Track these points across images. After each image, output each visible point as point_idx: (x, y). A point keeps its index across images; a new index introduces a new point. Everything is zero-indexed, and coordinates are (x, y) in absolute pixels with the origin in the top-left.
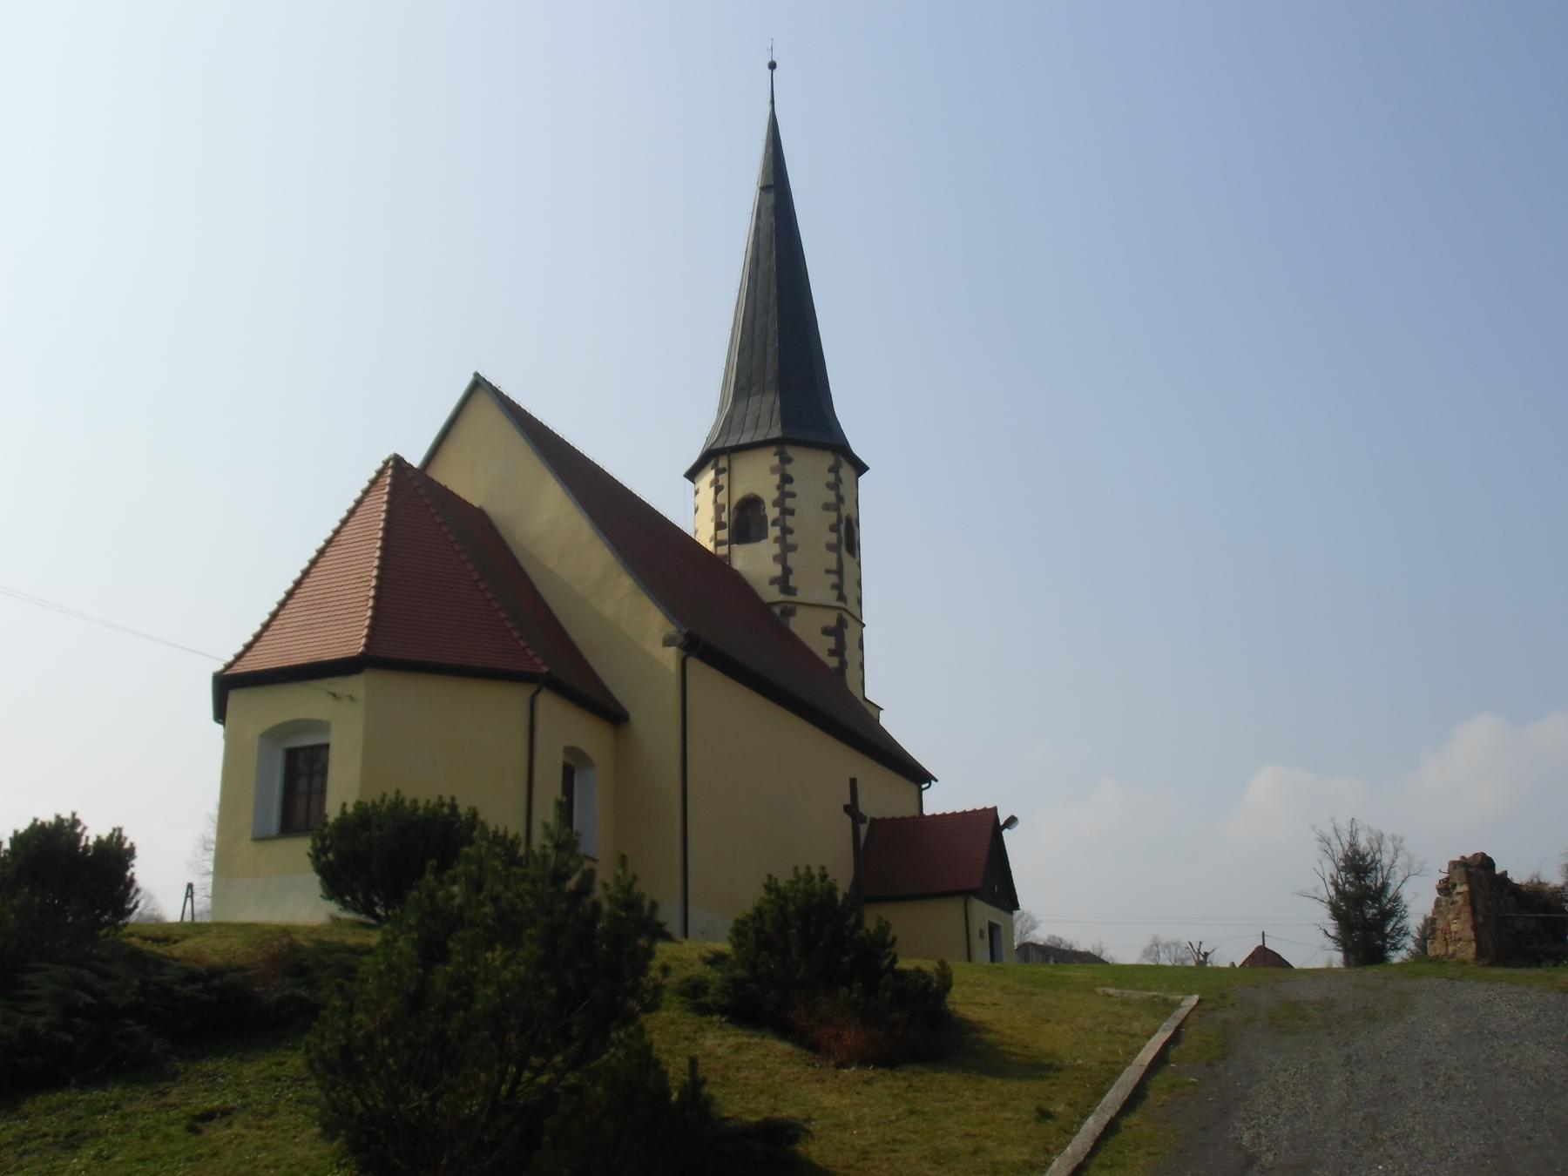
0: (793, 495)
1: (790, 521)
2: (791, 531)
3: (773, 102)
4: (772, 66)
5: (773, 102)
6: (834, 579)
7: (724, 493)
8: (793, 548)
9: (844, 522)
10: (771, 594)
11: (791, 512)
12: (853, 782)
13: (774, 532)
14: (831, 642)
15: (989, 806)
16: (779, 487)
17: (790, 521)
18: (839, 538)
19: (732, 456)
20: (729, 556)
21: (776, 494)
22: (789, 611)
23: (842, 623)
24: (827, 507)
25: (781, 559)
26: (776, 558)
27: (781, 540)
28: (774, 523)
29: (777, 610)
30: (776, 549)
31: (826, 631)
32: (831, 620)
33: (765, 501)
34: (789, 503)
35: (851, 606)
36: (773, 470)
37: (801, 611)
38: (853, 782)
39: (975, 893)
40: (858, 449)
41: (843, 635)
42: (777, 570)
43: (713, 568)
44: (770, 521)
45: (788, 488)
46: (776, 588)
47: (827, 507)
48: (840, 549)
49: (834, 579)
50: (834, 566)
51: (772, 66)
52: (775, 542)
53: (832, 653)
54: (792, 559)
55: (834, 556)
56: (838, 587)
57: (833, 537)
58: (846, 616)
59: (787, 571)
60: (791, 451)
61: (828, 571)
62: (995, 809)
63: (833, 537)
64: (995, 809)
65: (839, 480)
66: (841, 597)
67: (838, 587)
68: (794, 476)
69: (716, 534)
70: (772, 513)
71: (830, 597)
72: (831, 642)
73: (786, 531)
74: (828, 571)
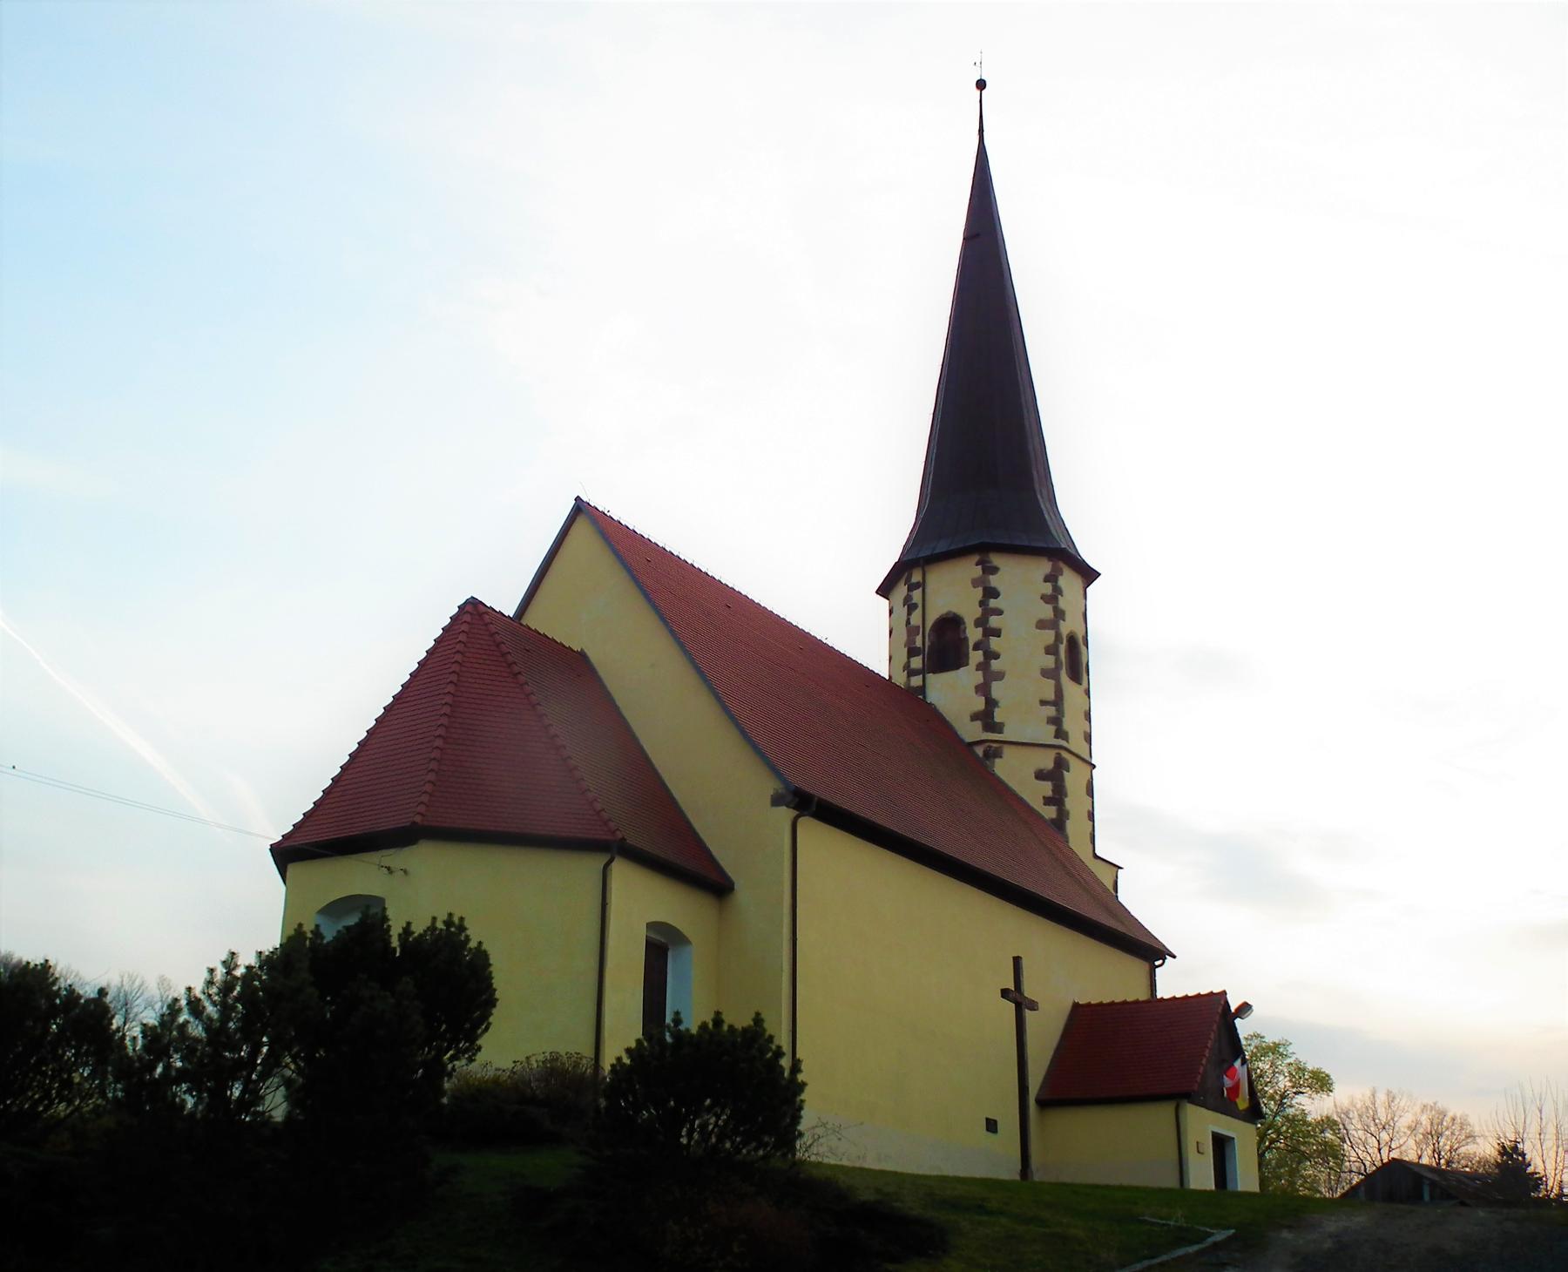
0: (999, 612)
1: (994, 643)
2: (997, 656)
4: (981, 85)
6: (1051, 711)
9: (1065, 641)
10: (971, 731)
11: (997, 633)
12: (1017, 961)
13: (976, 657)
14: (1047, 788)
16: (982, 603)
17: (994, 643)
18: (1058, 661)
19: (926, 568)
20: (922, 689)
21: (978, 612)
22: (993, 753)
24: (1041, 625)
25: (983, 689)
27: (983, 667)
28: (977, 647)
29: (979, 751)
30: (979, 677)
31: (1041, 775)
32: (1047, 761)
33: (966, 620)
34: (994, 621)
35: (1076, 743)
37: (1008, 751)
38: (1017, 961)
42: (979, 704)
45: (993, 603)
46: (978, 724)
47: (1041, 625)
49: (1051, 711)
50: (1051, 696)
51: (981, 85)
52: (977, 670)
53: (1048, 801)
54: (997, 689)
56: (1056, 721)
58: (1065, 755)
59: (991, 704)
60: (996, 560)
61: (1043, 703)
62: (1224, 993)
63: (1049, 661)
65: (1057, 591)
66: (1061, 733)
68: (1000, 588)
70: (973, 634)
71: (1047, 734)
72: (1047, 788)
73: (991, 655)
74: (1043, 703)
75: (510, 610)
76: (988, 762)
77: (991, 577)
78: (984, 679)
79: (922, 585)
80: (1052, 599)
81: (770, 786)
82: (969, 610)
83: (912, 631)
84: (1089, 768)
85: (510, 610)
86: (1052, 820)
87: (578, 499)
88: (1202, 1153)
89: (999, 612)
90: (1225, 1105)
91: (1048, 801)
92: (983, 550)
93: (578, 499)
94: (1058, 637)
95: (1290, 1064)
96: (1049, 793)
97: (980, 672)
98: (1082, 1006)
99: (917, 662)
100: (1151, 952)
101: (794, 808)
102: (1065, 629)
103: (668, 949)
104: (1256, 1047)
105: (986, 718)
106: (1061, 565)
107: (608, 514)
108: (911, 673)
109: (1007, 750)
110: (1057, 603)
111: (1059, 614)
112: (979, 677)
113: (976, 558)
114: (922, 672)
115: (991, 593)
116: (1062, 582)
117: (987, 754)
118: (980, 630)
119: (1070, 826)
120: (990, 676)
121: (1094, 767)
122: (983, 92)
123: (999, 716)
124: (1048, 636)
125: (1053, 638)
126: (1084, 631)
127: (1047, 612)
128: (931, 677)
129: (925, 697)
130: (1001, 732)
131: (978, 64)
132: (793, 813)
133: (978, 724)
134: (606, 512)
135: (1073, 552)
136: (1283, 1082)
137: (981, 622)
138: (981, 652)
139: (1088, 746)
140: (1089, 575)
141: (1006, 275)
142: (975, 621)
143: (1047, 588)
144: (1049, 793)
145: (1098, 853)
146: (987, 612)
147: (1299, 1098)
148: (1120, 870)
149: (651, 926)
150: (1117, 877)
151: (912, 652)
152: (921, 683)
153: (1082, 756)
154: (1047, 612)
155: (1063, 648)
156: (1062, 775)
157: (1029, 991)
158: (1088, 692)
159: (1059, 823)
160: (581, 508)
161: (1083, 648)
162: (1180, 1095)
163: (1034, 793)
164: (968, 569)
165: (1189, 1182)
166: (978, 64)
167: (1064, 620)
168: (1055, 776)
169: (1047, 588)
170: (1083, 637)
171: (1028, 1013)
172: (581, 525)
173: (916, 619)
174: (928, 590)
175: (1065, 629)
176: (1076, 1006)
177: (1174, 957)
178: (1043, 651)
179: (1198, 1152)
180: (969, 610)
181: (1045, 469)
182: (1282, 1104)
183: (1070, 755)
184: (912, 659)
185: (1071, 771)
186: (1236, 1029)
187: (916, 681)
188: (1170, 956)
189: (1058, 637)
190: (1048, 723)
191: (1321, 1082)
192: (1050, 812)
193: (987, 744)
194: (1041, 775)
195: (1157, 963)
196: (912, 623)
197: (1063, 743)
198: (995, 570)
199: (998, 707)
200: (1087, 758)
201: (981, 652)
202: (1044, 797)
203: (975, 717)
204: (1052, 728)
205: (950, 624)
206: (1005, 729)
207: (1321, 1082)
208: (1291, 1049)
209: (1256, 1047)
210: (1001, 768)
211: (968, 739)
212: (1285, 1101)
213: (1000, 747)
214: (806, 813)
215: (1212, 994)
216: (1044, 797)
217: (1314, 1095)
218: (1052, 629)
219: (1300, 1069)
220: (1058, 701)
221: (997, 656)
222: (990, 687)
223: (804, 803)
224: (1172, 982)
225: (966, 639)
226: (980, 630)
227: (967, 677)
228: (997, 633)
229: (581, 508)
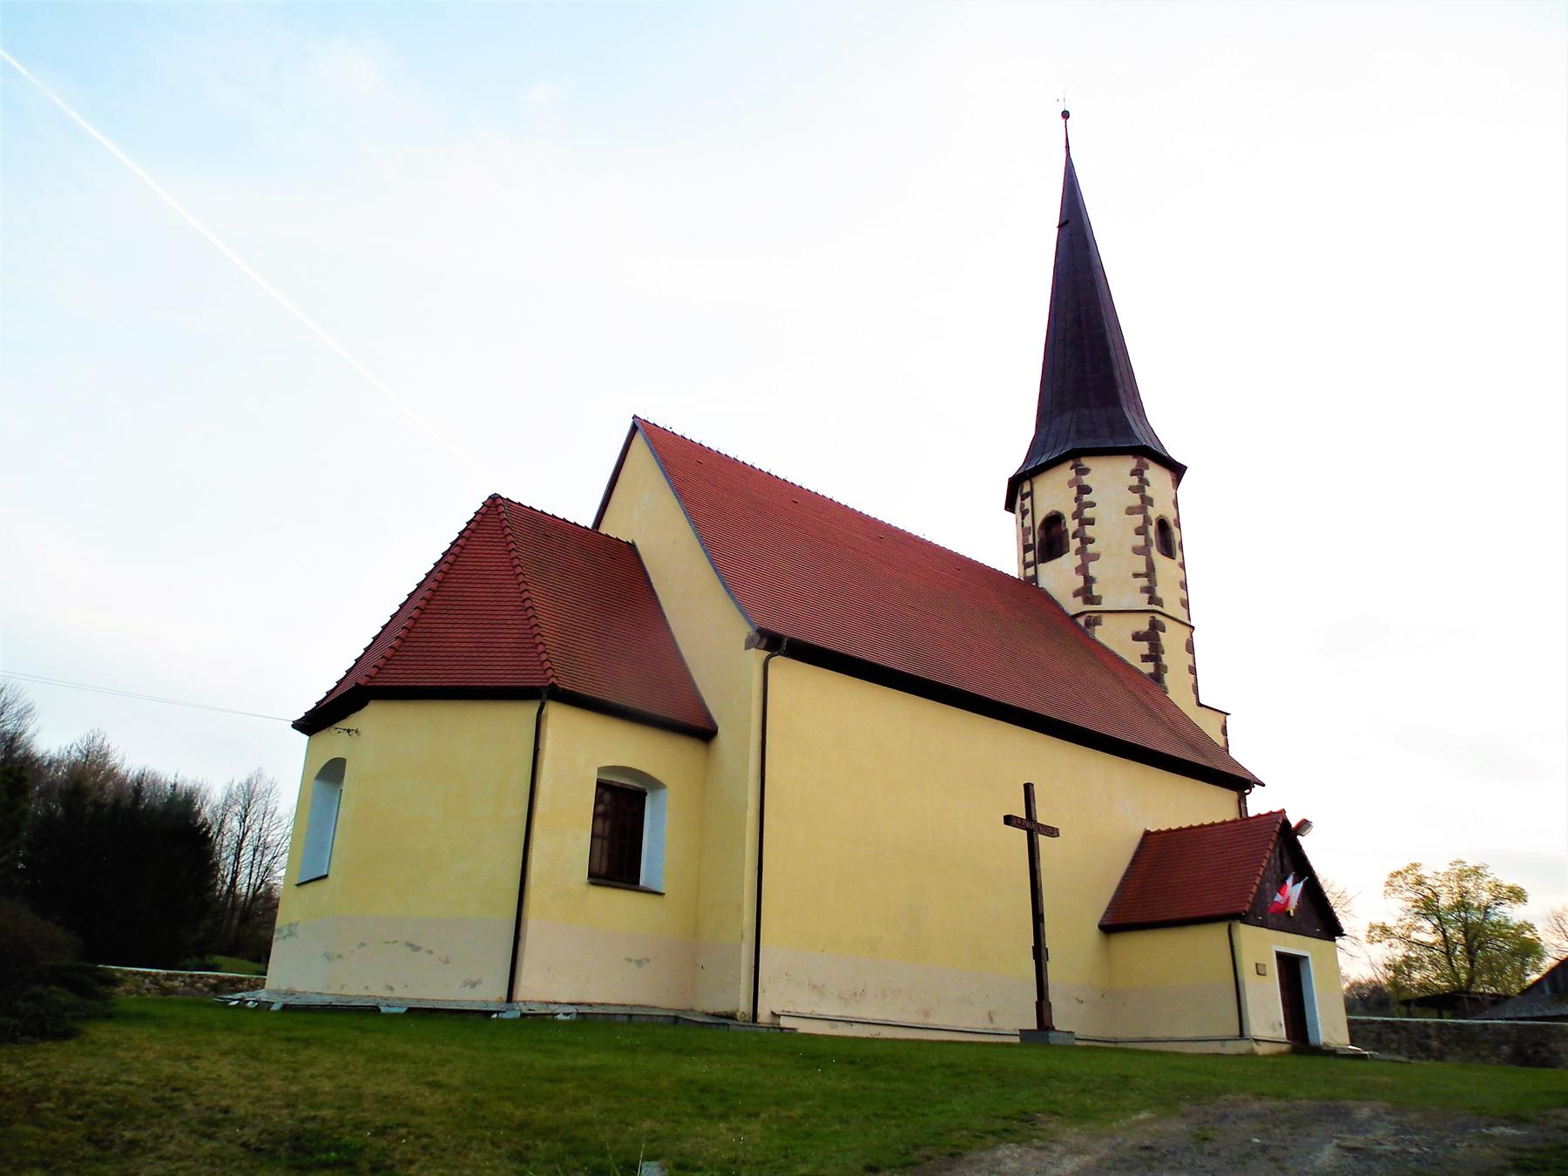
0: (1092, 505)
1: (1089, 531)
2: (1092, 541)
3: (1067, 147)
4: (1066, 115)
5: (1067, 147)
6: (1144, 582)
7: (1028, 517)
8: (1096, 557)
9: (1154, 523)
10: (1073, 606)
11: (1091, 522)
12: (1028, 788)
13: (1075, 544)
14: (1144, 647)
15: (1275, 810)
16: (1077, 500)
17: (1089, 531)
18: (1147, 540)
19: (1033, 480)
20: (1035, 578)
21: (1074, 507)
22: (1093, 622)
23: (1156, 627)
24: (1131, 511)
25: (1082, 570)
26: (1077, 570)
27: (1081, 551)
28: (1074, 536)
29: (1081, 621)
30: (1078, 560)
31: (1137, 637)
32: (1143, 624)
33: (1066, 516)
34: (1088, 513)
35: (1171, 606)
36: (1071, 484)
37: (1105, 618)
38: (1028, 788)
39: (1245, 919)
40: (1175, 452)
41: (1158, 639)
42: (1079, 582)
43: (1027, 590)
44: (1070, 534)
45: (1086, 498)
46: (1080, 599)
47: (1131, 511)
48: (1149, 551)
49: (1144, 582)
50: (1143, 569)
51: (1066, 115)
52: (1076, 554)
53: (1145, 658)
54: (1093, 569)
55: (1143, 558)
56: (1149, 590)
57: (1140, 541)
58: (1158, 617)
59: (1089, 580)
60: (1086, 462)
61: (1136, 575)
62: (1283, 812)
63: (1140, 541)
64: (1283, 812)
65: (1144, 482)
66: (1153, 599)
67: (1149, 590)
68: (1092, 485)
69: (1024, 557)
70: (1071, 525)
71: (1142, 602)
72: (1144, 647)
73: (1087, 541)
74: (1136, 575)
75: (587, 521)
76: (1088, 630)
77: (1083, 477)
78: (1082, 561)
79: (1031, 494)
80: (1139, 489)
81: (744, 631)
82: (1067, 507)
83: (1025, 531)
84: (1187, 630)
85: (587, 521)
86: (1151, 674)
87: (635, 417)
88: (1264, 975)
89: (1092, 505)
90: (1283, 922)
91: (1145, 658)
92: (1074, 455)
93: (635, 417)
94: (1147, 520)
95: (1490, 882)
96: (1147, 652)
97: (1079, 556)
98: (1154, 833)
99: (1030, 556)
100: (1241, 783)
101: (765, 649)
102: (1154, 513)
103: (646, 794)
104: (1460, 870)
105: (1086, 594)
106: (1146, 460)
107: (671, 430)
108: (1027, 565)
109: (1105, 618)
110: (1144, 492)
111: (1147, 501)
112: (1078, 560)
113: (1071, 463)
114: (1034, 564)
115: (1084, 490)
116: (1147, 474)
117: (1088, 624)
118: (1077, 521)
119: (1168, 679)
120: (1086, 558)
121: (1193, 628)
122: (1068, 121)
123: (1096, 591)
124: (1138, 520)
125: (1142, 521)
126: (1176, 514)
127: (1135, 500)
128: (1041, 567)
129: (1037, 583)
130: (1099, 604)
131: (1061, 100)
132: (767, 653)
133: (1080, 599)
134: (668, 429)
135: (1160, 451)
136: (1485, 897)
137: (1077, 515)
138: (1078, 539)
139: (1186, 611)
140: (1177, 470)
141: (1092, 244)
142: (1073, 515)
143: (1135, 481)
144: (1147, 652)
145: (1202, 702)
146: (1082, 506)
147: (1501, 908)
148: (1228, 717)
149: (602, 770)
150: (1226, 722)
151: (1026, 549)
152: (1034, 573)
153: (1183, 620)
154: (1135, 500)
155: (1152, 530)
156: (1157, 634)
157: (1042, 817)
158: (1182, 566)
159: (1158, 677)
160: (638, 427)
161: (1175, 530)
162: (1231, 917)
163: (1133, 653)
164: (1065, 473)
165: (1246, 1005)
166: (1061, 100)
167: (1152, 506)
168: (1151, 635)
169: (1135, 481)
170: (1175, 520)
171: (1042, 840)
172: (639, 439)
173: (1028, 521)
174: (1034, 497)
175: (1154, 513)
176: (1147, 834)
177: (1264, 785)
178: (1134, 532)
179: (1258, 973)
180: (1067, 507)
181: (1132, 386)
182: (1486, 912)
183: (1164, 618)
184: (1027, 554)
185: (1167, 631)
186: (1301, 847)
187: (1030, 572)
188: (1259, 784)
189: (1147, 520)
190: (1141, 592)
191: (1518, 895)
192: (1148, 668)
193: (1087, 615)
194: (1137, 637)
195: (1247, 791)
196: (1025, 525)
197: (1154, 607)
198: (1086, 471)
199: (1095, 583)
200: (1187, 622)
201: (1078, 539)
202: (1142, 655)
203: (1076, 594)
204: (1146, 596)
205: (1054, 520)
206: (1103, 601)
207: (1518, 895)
208: (1489, 871)
209: (1460, 870)
210: (1102, 634)
211: (1072, 613)
212: (1489, 910)
213: (1100, 617)
214: (776, 653)
215: (1271, 813)
216: (1142, 655)
217: (1513, 905)
218: (1141, 513)
219: (1497, 885)
220: (1150, 572)
221: (1092, 541)
222: (1088, 567)
223: (773, 643)
224: (1258, 803)
225: (1066, 530)
226: (1077, 521)
227: (1069, 561)
228: (1091, 522)
229: (638, 427)
